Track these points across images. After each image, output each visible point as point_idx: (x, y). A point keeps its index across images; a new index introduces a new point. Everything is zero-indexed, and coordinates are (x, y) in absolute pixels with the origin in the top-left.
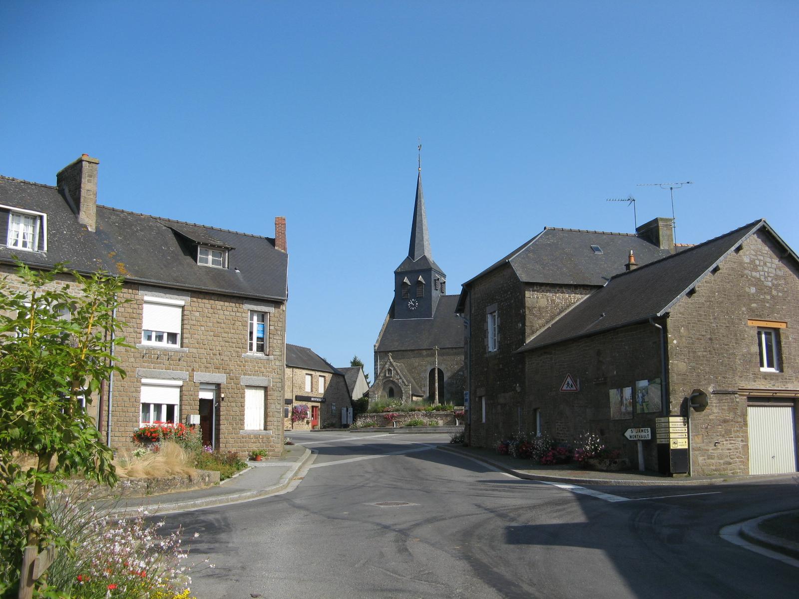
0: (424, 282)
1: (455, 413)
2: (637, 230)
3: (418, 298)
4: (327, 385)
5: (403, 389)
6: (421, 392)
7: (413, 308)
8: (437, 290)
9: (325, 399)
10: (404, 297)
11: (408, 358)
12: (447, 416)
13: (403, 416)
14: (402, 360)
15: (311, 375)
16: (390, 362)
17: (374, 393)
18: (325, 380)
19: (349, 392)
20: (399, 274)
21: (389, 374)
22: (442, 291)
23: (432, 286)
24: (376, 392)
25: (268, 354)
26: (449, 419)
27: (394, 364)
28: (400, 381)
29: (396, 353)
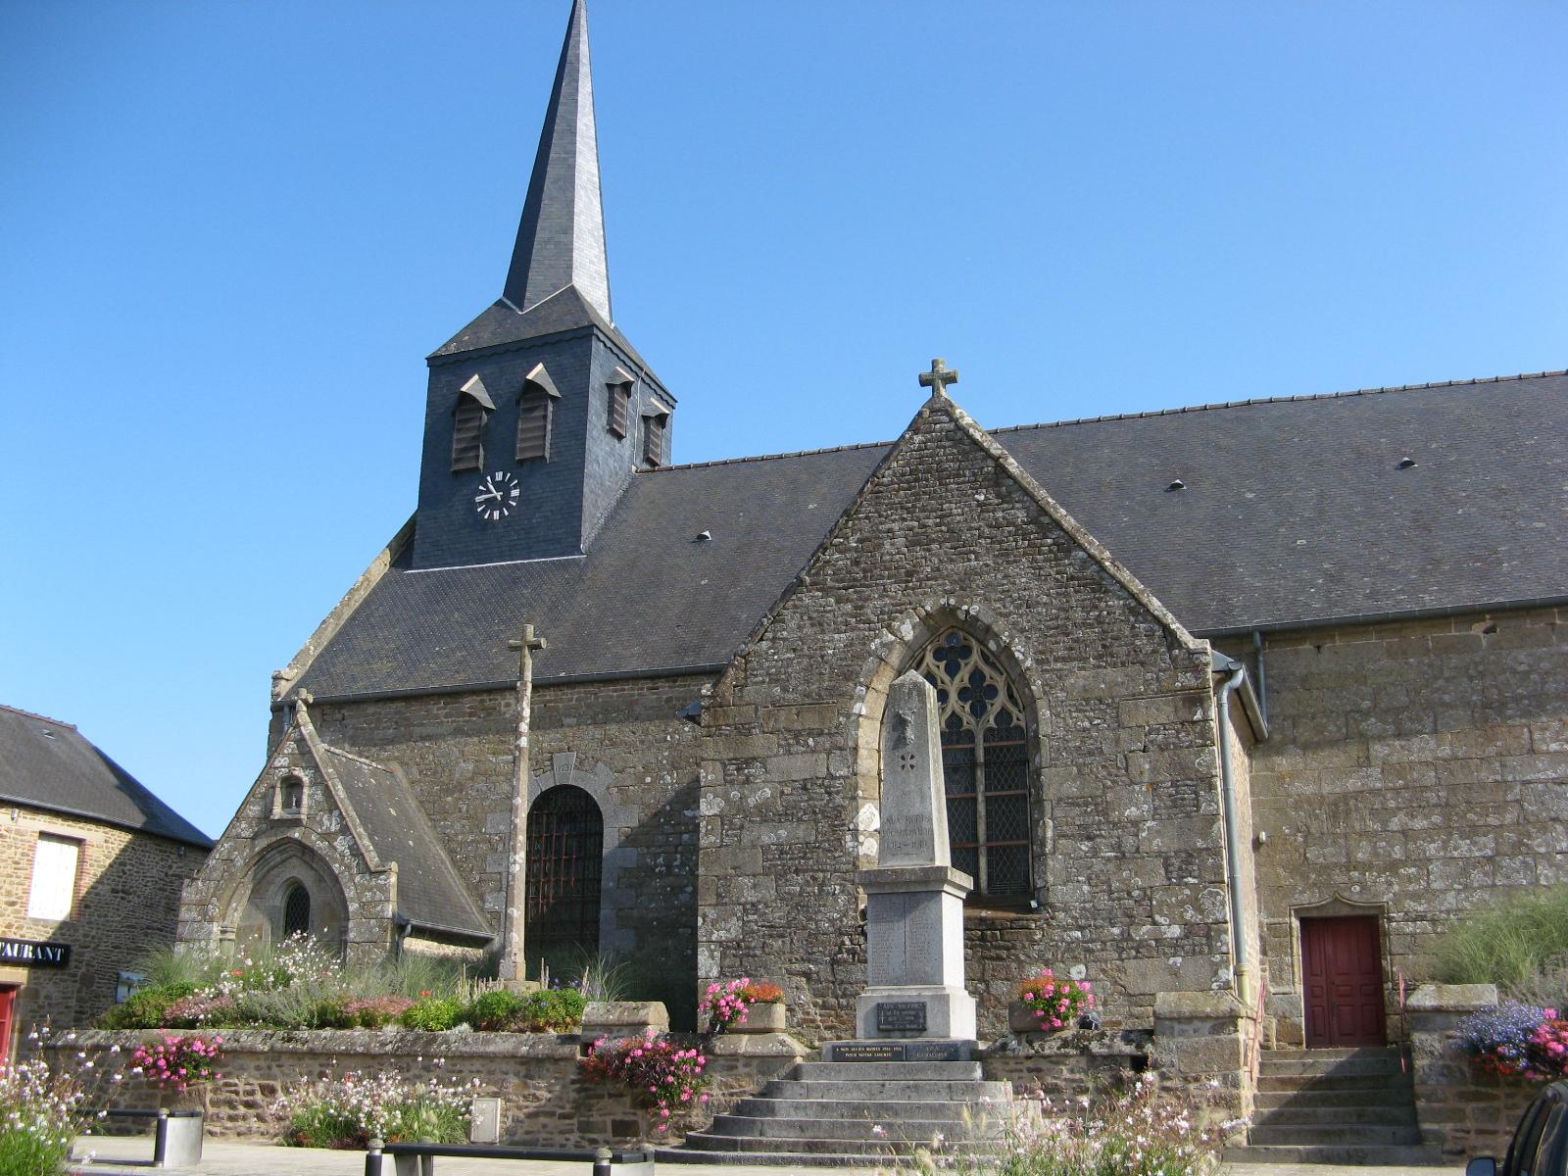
0: (553, 391)
1: (587, 1046)
2: (948, 995)
3: (521, 462)
4: (88, 881)
5: (350, 893)
6: (478, 917)
7: (496, 515)
8: (620, 437)
9: (67, 949)
10: (461, 466)
11: (423, 739)
12: (530, 1066)
13: (252, 1053)
14: (394, 751)
15: (79, 842)
16: (301, 741)
17: (204, 914)
18: (81, 861)
19: (1415, 1029)
20: (445, 366)
21: (286, 805)
22: (646, 451)
23: (591, 411)
24: (214, 910)
25: (689, 931)
26: (543, 1090)
27: (320, 748)
28: (341, 844)
29: (371, 709)
